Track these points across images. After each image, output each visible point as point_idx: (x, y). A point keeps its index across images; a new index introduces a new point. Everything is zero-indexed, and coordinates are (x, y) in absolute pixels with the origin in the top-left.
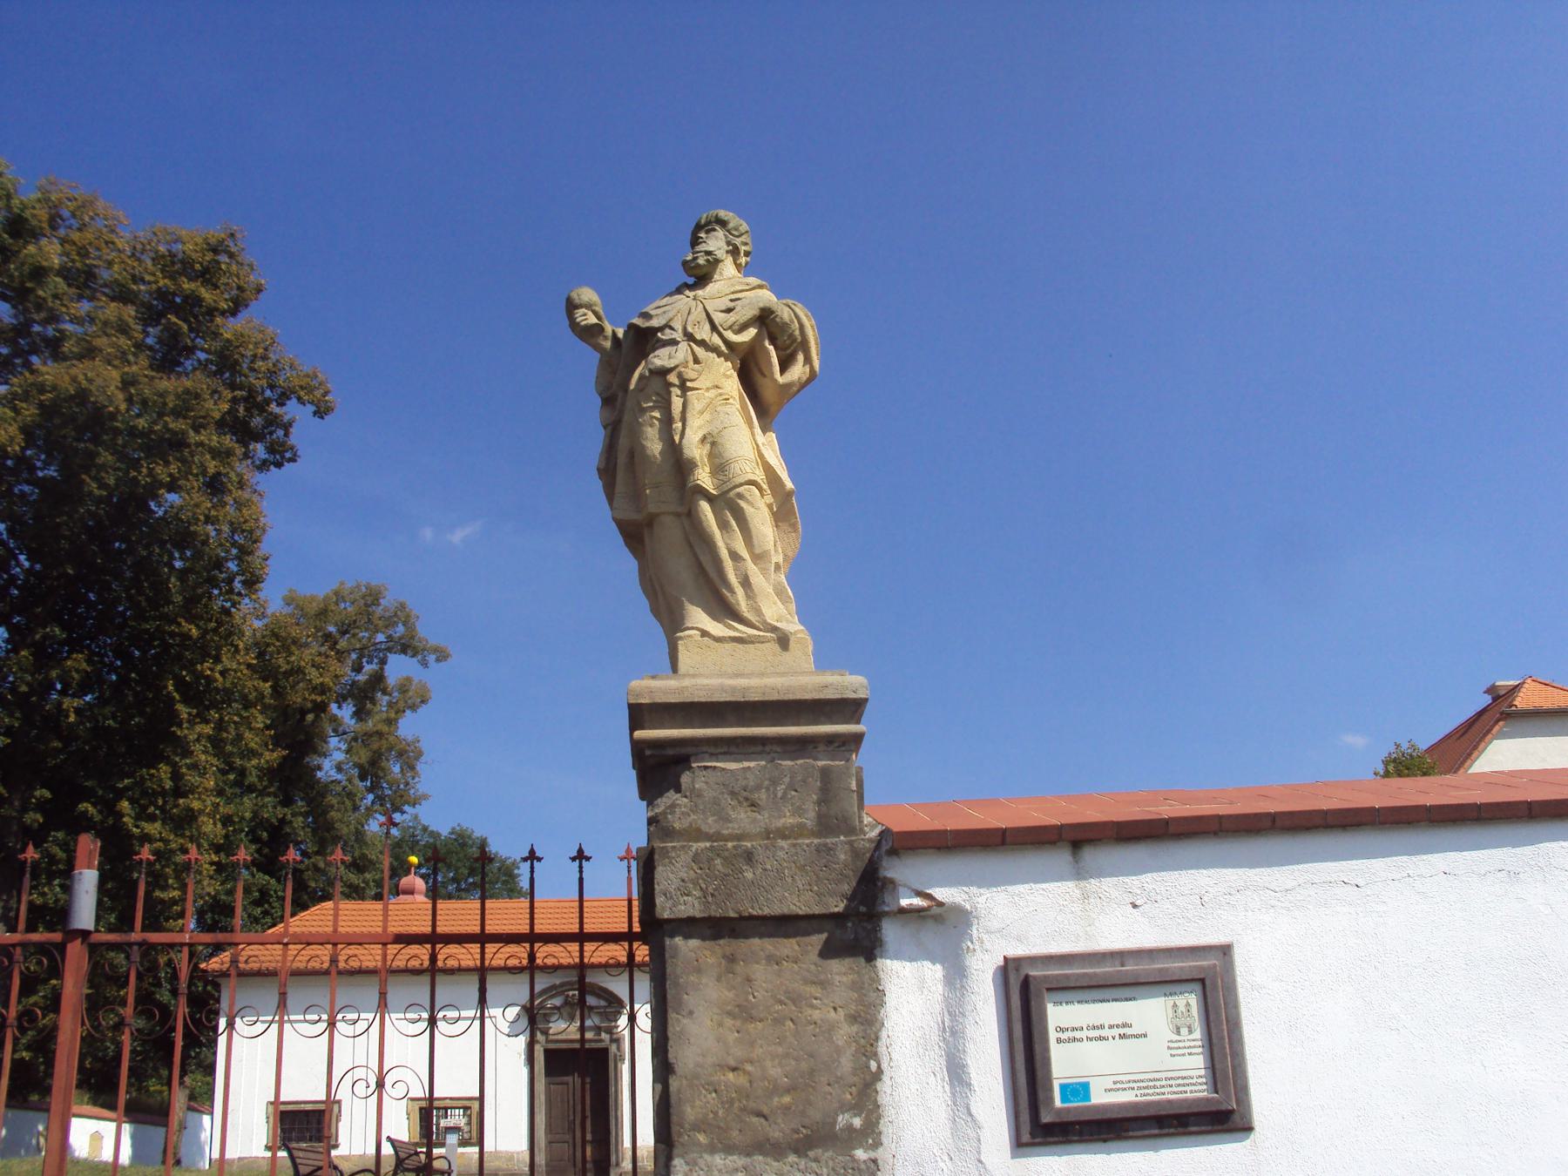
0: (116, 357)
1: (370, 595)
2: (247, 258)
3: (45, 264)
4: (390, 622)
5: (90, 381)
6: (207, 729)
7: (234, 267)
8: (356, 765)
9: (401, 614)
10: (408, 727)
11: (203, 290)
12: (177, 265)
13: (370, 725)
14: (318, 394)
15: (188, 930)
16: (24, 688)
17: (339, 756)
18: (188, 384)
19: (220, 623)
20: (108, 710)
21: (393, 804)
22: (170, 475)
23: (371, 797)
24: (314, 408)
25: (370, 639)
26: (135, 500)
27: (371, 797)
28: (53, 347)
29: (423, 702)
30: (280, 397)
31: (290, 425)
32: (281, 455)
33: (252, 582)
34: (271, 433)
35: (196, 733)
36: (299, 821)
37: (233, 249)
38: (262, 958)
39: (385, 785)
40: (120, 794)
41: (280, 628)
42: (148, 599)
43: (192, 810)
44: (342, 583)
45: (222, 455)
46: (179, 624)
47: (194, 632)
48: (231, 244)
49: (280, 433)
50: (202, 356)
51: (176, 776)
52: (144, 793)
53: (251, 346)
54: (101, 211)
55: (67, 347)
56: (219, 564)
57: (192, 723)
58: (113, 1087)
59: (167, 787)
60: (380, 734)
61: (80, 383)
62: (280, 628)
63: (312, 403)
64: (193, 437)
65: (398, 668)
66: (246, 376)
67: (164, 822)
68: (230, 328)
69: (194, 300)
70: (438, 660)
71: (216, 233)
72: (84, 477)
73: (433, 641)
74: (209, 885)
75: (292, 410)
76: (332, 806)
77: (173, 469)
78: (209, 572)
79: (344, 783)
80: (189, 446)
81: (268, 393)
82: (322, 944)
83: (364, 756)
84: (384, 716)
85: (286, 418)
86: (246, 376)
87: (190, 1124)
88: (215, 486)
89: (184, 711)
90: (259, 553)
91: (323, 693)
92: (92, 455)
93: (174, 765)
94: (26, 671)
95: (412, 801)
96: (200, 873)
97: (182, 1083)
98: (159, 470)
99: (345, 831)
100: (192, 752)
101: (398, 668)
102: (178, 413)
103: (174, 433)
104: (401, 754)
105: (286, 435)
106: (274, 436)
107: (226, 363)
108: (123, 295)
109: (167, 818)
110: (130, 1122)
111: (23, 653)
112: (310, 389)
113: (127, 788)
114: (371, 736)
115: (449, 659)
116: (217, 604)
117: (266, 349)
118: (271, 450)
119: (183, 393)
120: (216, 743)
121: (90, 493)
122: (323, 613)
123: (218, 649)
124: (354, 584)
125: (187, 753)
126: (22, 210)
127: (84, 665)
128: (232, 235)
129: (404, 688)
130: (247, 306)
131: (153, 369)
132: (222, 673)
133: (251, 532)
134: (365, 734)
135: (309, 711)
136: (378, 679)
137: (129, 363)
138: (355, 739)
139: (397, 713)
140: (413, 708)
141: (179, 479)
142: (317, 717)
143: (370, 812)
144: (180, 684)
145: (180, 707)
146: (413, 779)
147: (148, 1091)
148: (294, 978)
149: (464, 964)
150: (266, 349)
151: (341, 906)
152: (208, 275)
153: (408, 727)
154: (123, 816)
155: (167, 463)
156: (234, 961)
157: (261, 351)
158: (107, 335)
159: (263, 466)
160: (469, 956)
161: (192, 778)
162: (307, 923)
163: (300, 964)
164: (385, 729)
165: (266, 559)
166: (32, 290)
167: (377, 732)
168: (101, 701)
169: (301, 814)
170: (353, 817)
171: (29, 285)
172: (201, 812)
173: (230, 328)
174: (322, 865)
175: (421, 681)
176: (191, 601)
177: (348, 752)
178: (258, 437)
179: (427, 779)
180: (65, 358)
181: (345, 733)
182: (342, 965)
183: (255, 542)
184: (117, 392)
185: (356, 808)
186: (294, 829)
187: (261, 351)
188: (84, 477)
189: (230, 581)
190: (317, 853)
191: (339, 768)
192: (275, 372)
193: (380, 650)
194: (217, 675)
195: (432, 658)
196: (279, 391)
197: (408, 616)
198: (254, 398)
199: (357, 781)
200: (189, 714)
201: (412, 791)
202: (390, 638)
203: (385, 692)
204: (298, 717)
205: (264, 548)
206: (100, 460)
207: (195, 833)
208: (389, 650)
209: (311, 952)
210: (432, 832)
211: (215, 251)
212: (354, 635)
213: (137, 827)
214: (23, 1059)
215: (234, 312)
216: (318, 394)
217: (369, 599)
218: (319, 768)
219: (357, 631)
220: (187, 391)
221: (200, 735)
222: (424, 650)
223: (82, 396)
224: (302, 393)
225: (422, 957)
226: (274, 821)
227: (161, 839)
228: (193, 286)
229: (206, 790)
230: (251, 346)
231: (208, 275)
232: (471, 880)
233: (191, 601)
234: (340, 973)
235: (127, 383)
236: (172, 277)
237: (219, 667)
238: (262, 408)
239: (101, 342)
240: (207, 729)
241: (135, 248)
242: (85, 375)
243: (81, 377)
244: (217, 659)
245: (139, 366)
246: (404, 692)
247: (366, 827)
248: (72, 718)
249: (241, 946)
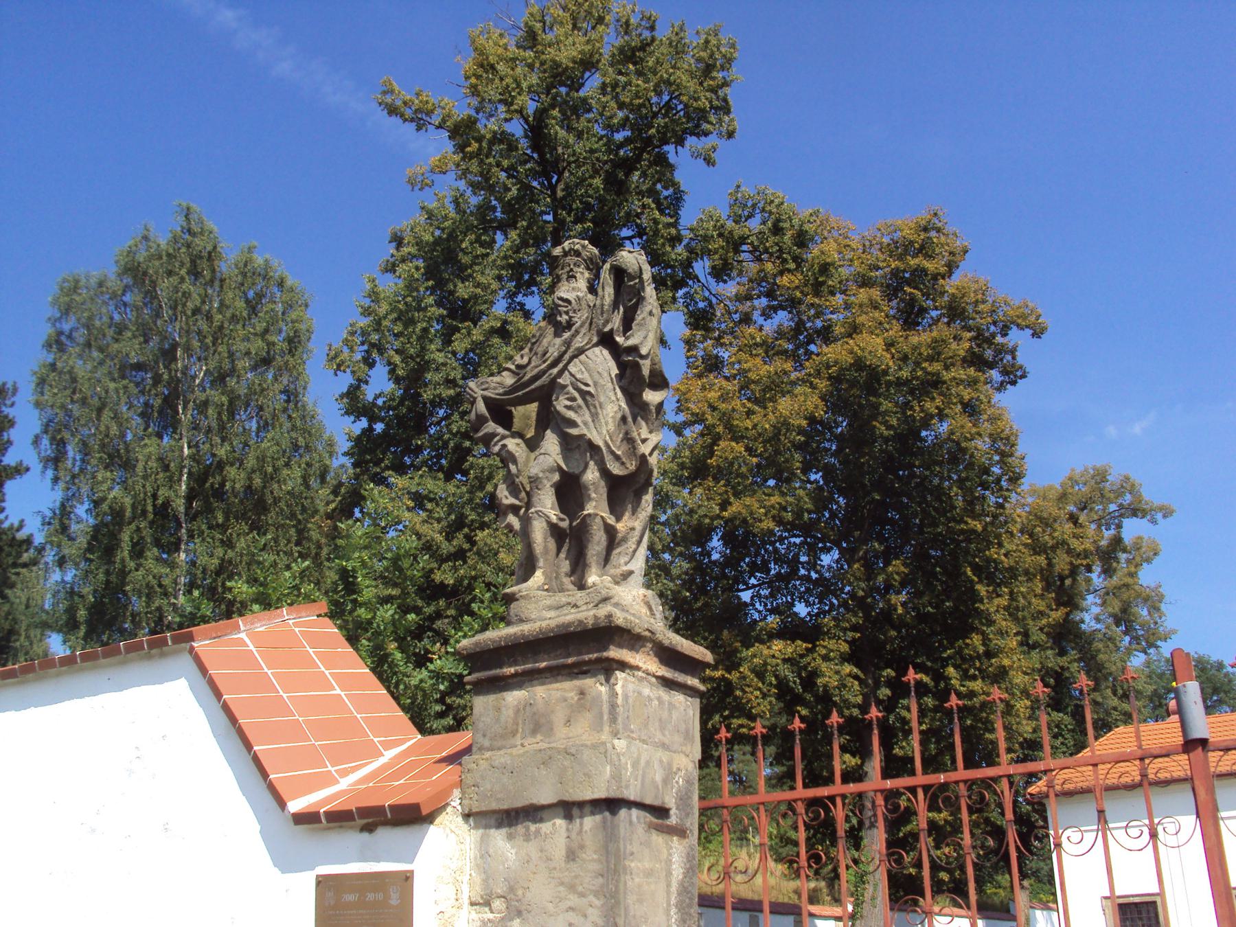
0: (876, 328)
1: (1098, 474)
2: (949, 229)
3: (829, 260)
4: (1119, 493)
5: (863, 350)
6: (1004, 601)
7: (943, 239)
8: (1111, 615)
9: (1128, 485)
10: (1147, 577)
11: (925, 262)
12: (903, 249)
13: (1115, 580)
14: (1032, 319)
15: (1006, 766)
16: (861, 593)
17: (1096, 610)
18: (935, 334)
19: (995, 517)
20: (925, 599)
21: (1147, 642)
22: (937, 408)
23: (1127, 639)
24: (1031, 332)
25: (1104, 510)
26: (908, 436)
27: (1127, 639)
28: (826, 334)
29: (1155, 554)
30: (1002, 330)
31: (1015, 350)
32: (1013, 375)
33: (1015, 479)
34: (1001, 360)
35: (994, 605)
36: (1075, 667)
37: (940, 225)
38: (1075, 780)
39: (1138, 627)
40: (945, 663)
41: (1042, 511)
42: (936, 509)
43: (1004, 667)
44: (1073, 470)
45: (973, 383)
46: (966, 523)
47: (979, 527)
48: (937, 222)
49: (1009, 357)
50: (934, 314)
51: (986, 640)
52: (963, 659)
53: (972, 295)
54: (834, 225)
55: (838, 330)
56: (986, 471)
57: (990, 599)
58: (964, 894)
59: (981, 651)
60: (1126, 586)
61: (856, 354)
62: (1042, 511)
63: (1027, 327)
64: (946, 376)
65: (1132, 529)
66: (974, 319)
67: (983, 679)
68: (951, 285)
69: (920, 272)
70: (1165, 516)
71: (923, 216)
72: (874, 423)
73: (1156, 503)
74: (1027, 724)
75: (1016, 337)
76: (1099, 651)
77: (938, 402)
78: (980, 477)
79: (1103, 630)
80: (944, 382)
81: (992, 328)
82: (1167, 755)
83: (1116, 606)
84: (1126, 570)
85: (1011, 345)
86: (974, 319)
87: (1031, 915)
88: (971, 409)
89: (982, 589)
90: (1018, 454)
91: (1086, 557)
92: (876, 406)
93: (983, 633)
94: (860, 579)
95: (1163, 637)
96: (1018, 716)
97: (1022, 887)
98: (928, 405)
99: (1113, 668)
100: (995, 622)
101: (1132, 529)
102: (931, 359)
103: (933, 374)
104: (1146, 600)
105: (1014, 358)
106: (1005, 361)
107: (955, 312)
108: (865, 282)
109: (984, 675)
110: (983, 918)
111: (855, 566)
112: (1024, 317)
113: (950, 657)
114: (1120, 588)
115: (1174, 514)
116: (992, 500)
117: (983, 294)
118: (1005, 372)
119: (932, 342)
120: (1012, 612)
121: (881, 434)
122: (1063, 497)
123: (998, 536)
124: (1083, 469)
125: (991, 623)
126: (801, 226)
127: (902, 569)
128: (936, 214)
129: (1137, 546)
130: (958, 267)
131: (905, 331)
132: (1006, 555)
133: (1008, 439)
134: (1115, 588)
135: (1067, 577)
136: (1117, 541)
137: (887, 331)
138: (1107, 594)
139: (1136, 566)
140: (1148, 560)
141: (944, 409)
142: (1074, 580)
143: (1129, 652)
144: (977, 569)
145: (978, 587)
146: (1160, 618)
147: (986, 893)
148: (1107, 792)
149: (1175, 775)
150: (983, 294)
151: (1141, 729)
152: (925, 249)
153: (1147, 577)
154: (950, 679)
155: (933, 399)
156: (1050, 786)
157: (980, 296)
158: (866, 313)
159: (1001, 388)
160: (1180, 768)
161: (997, 642)
162: (1105, 747)
163: (1112, 780)
164: (1129, 580)
165: (1023, 458)
166: (823, 283)
167: (1124, 585)
168: (918, 594)
169: (1075, 660)
170: (1115, 657)
171: (820, 279)
172: (1011, 667)
173: (951, 285)
174: (1100, 699)
175: (1149, 538)
176: (971, 502)
177: (1104, 604)
178: (991, 366)
179: (1171, 617)
180: (836, 340)
181: (1096, 591)
182: (1058, 788)
183: (1013, 445)
184: (884, 353)
185: (1118, 649)
186: (1072, 673)
187: (980, 296)
188: (874, 423)
189: (998, 481)
190: (1094, 690)
191: (1097, 619)
192: (994, 311)
193: (1115, 517)
194: (1003, 557)
195: (1159, 516)
196: (1001, 324)
197: (1133, 485)
198: (983, 335)
199: (1114, 627)
200: (987, 591)
201: (1161, 629)
202: (1121, 506)
203: (1125, 551)
204: (1058, 583)
205: (1020, 450)
206: (882, 409)
207: (1009, 686)
208: (1122, 516)
209: (1065, 776)
210: (327, 813)
211: (925, 229)
212: (1091, 509)
213: (964, 686)
214: (911, 874)
215: (950, 273)
216: (1032, 319)
217: (1098, 478)
218: (1082, 621)
219: (1094, 505)
220: (935, 341)
221: (998, 606)
222: (1151, 510)
223: (859, 364)
224: (1019, 321)
225: (1133, 773)
226: (1057, 668)
227: (984, 693)
228: (917, 261)
229: (1012, 649)
230: (972, 295)
231: (925, 249)
232: (1215, 698)
233: (971, 502)
234: (1150, 784)
235: (889, 345)
236: (901, 258)
237: (1003, 551)
238: (989, 341)
239: (862, 319)
240: (1004, 601)
241: (864, 245)
242: (858, 346)
243: (856, 348)
244: (1000, 545)
245: (895, 329)
246: (1138, 549)
247: (1129, 664)
248: (900, 611)
249: (1054, 773)
